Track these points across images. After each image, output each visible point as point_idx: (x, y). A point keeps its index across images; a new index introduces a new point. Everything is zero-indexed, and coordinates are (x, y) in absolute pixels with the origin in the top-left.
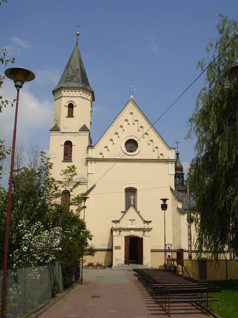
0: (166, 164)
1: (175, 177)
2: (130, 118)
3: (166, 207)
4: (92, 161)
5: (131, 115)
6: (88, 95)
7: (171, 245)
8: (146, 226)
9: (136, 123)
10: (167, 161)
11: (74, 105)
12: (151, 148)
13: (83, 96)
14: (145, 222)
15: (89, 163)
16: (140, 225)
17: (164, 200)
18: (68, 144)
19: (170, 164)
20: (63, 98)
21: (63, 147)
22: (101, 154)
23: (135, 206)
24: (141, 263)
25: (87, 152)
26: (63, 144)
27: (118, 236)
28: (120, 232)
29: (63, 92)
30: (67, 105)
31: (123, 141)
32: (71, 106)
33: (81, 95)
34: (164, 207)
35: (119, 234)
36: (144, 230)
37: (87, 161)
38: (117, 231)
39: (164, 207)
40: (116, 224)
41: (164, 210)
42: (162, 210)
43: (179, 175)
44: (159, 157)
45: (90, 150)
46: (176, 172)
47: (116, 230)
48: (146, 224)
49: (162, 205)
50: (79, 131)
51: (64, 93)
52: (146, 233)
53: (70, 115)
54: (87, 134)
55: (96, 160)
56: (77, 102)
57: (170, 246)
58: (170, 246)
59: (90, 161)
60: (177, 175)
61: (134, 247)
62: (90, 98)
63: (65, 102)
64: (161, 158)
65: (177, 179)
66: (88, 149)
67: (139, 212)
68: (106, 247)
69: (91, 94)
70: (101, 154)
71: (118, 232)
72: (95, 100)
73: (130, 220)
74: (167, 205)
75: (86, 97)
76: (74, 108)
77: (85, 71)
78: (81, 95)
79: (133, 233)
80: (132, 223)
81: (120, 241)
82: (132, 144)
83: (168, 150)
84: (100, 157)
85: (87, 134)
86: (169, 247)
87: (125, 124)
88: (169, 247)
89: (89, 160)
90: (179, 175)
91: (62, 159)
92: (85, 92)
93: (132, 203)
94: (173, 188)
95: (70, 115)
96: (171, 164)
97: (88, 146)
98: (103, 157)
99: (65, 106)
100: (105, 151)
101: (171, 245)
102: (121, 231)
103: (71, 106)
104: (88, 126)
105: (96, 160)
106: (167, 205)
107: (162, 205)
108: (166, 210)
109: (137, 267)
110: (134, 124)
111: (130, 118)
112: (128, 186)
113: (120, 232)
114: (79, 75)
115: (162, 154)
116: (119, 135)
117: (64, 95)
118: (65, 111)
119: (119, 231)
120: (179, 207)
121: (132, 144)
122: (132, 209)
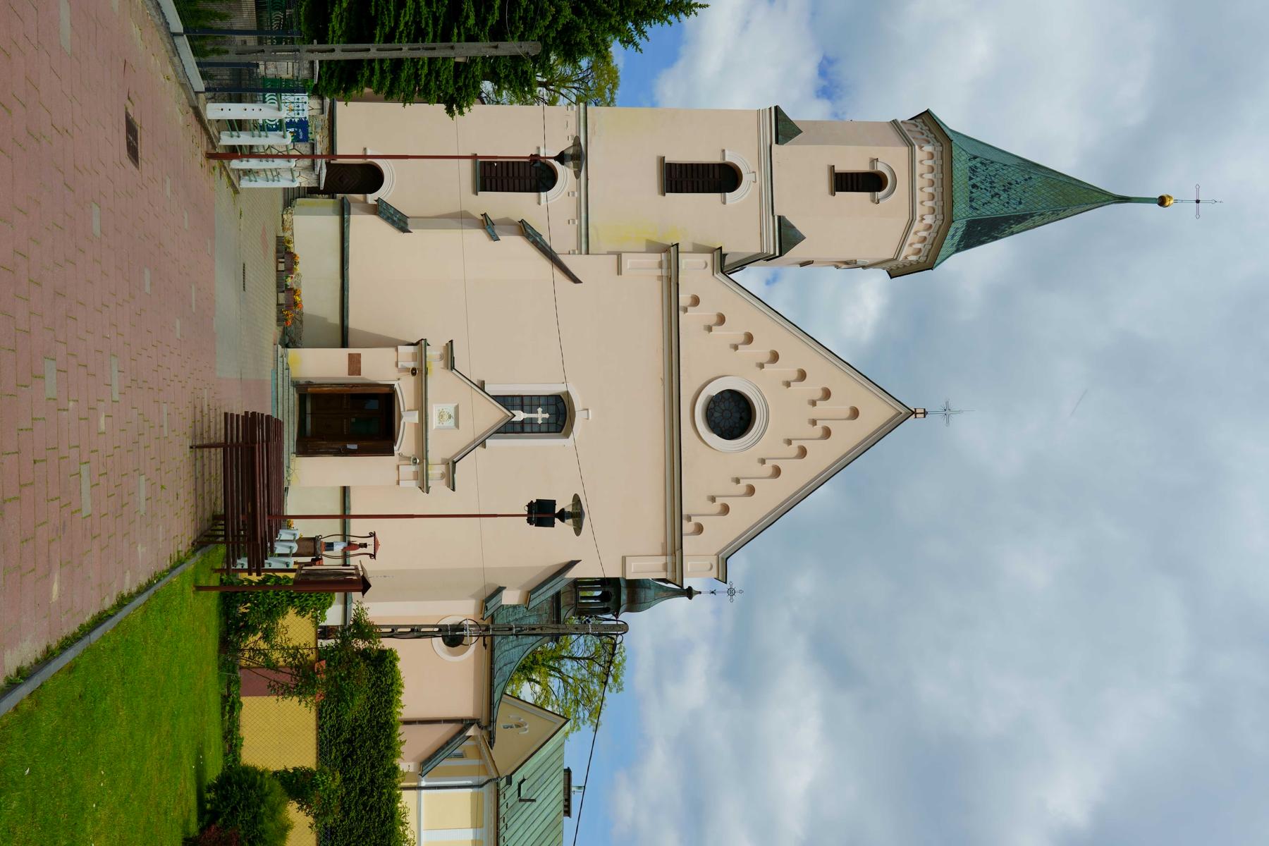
0: (665, 545)
1: (604, 582)
2: (835, 408)
3: (540, 523)
4: (669, 267)
5: (847, 413)
6: (919, 246)
7: (373, 556)
8: (436, 471)
9: (818, 430)
10: (675, 549)
11: (880, 194)
12: (722, 486)
13: (917, 226)
14: (452, 465)
15: (656, 258)
16: (438, 451)
17: (576, 515)
18: (721, 178)
19: (662, 560)
20: (904, 150)
21: (717, 159)
22: (696, 301)
23: (509, 429)
24: (307, 447)
25: (698, 249)
26: (728, 159)
27: (397, 365)
28: (414, 372)
29: (928, 148)
30: (880, 168)
31: (750, 382)
32: (871, 182)
33: (918, 218)
34: (542, 513)
35: (406, 369)
36: (421, 458)
37: (666, 249)
38: (415, 360)
39: (542, 513)
40: (441, 357)
41: (530, 512)
42: (530, 505)
43: (614, 598)
44: (689, 519)
45: (708, 257)
46: (623, 584)
47: (421, 357)
48: (442, 469)
49: (553, 503)
50: (779, 217)
51: (924, 153)
52: (409, 470)
53: (844, 182)
54: (768, 247)
55: (672, 283)
56: (894, 202)
57: (370, 550)
58: (370, 550)
59: (669, 261)
60: (610, 590)
61: (357, 420)
62: (909, 255)
63: (891, 159)
64: (688, 527)
65: (597, 589)
66: (712, 251)
67: (483, 444)
68: (353, 323)
69: (923, 259)
70: (696, 301)
71: (411, 365)
72: (928, 112)
73: (457, 408)
74: (552, 525)
75: (911, 238)
76: (867, 195)
77: (1012, 233)
78: (918, 218)
79: (407, 421)
80: (446, 417)
81: (379, 367)
82: (732, 415)
83: (718, 555)
84: (684, 299)
85: (768, 247)
86: (365, 545)
87: (811, 388)
88: (365, 545)
89: (671, 252)
90: (614, 598)
91: (672, 158)
92: (929, 247)
93: (520, 416)
94: (573, 574)
95: (844, 182)
96: (666, 565)
97: (724, 251)
98: (686, 310)
99: (874, 161)
100: (704, 313)
101: (373, 556)
102: (414, 374)
103: (871, 182)
104: (797, 253)
105: (672, 283)
106: (552, 525)
107: (553, 503)
108: (530, 521)
109: (286, 436)
110: (814, 422)
111: (835, 408)
112: (578, 404)
113: (414, 372)
114: (994, 209)
115: (699, 529)
116: (769, 368)
117: (919, 155)
118: (855, 163)
119: (414, 369)
120: (504, 592)
121: (732, 415)
122: (497, 414)
